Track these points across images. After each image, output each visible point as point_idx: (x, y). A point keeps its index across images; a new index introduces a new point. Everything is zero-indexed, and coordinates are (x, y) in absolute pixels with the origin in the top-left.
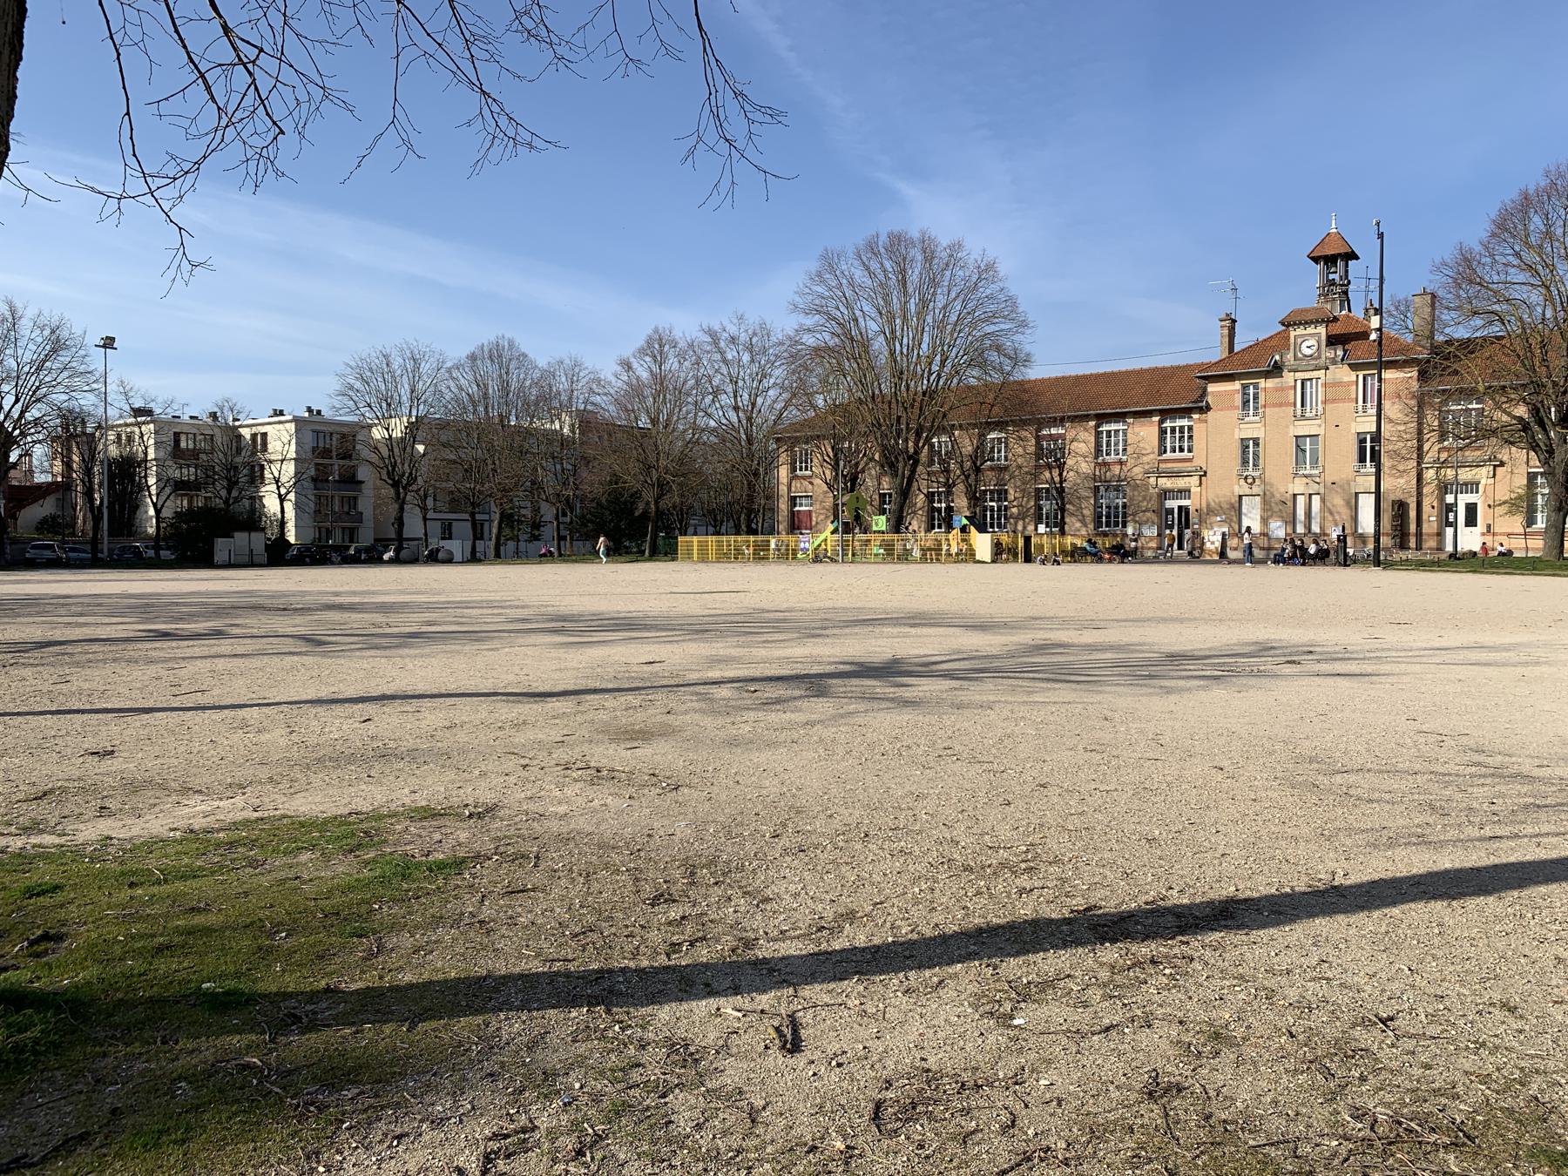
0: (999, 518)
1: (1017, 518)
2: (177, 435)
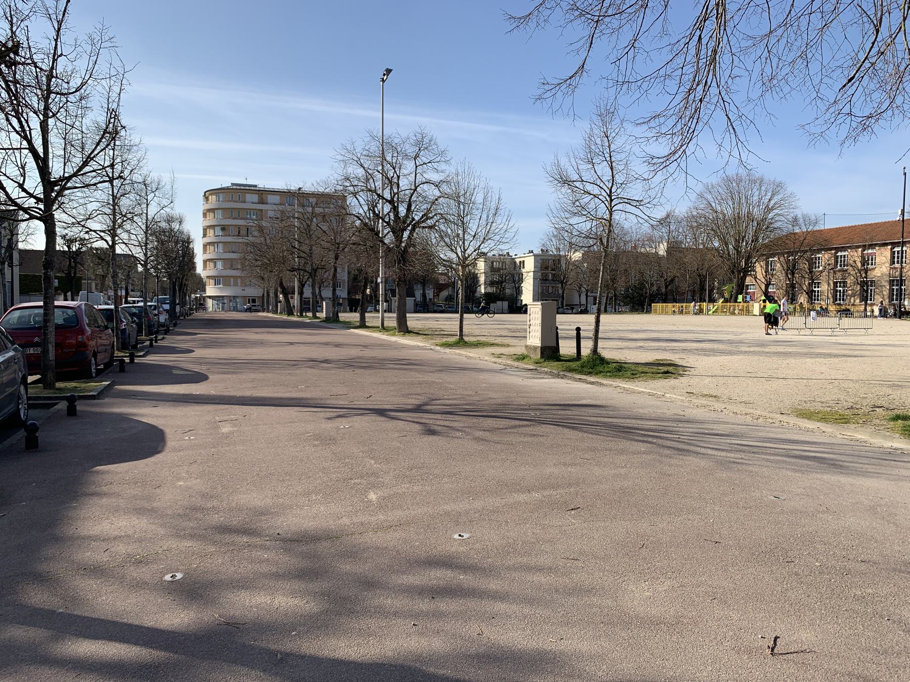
0: (843, 296)
1: (851, 296)
2: (492, 263)
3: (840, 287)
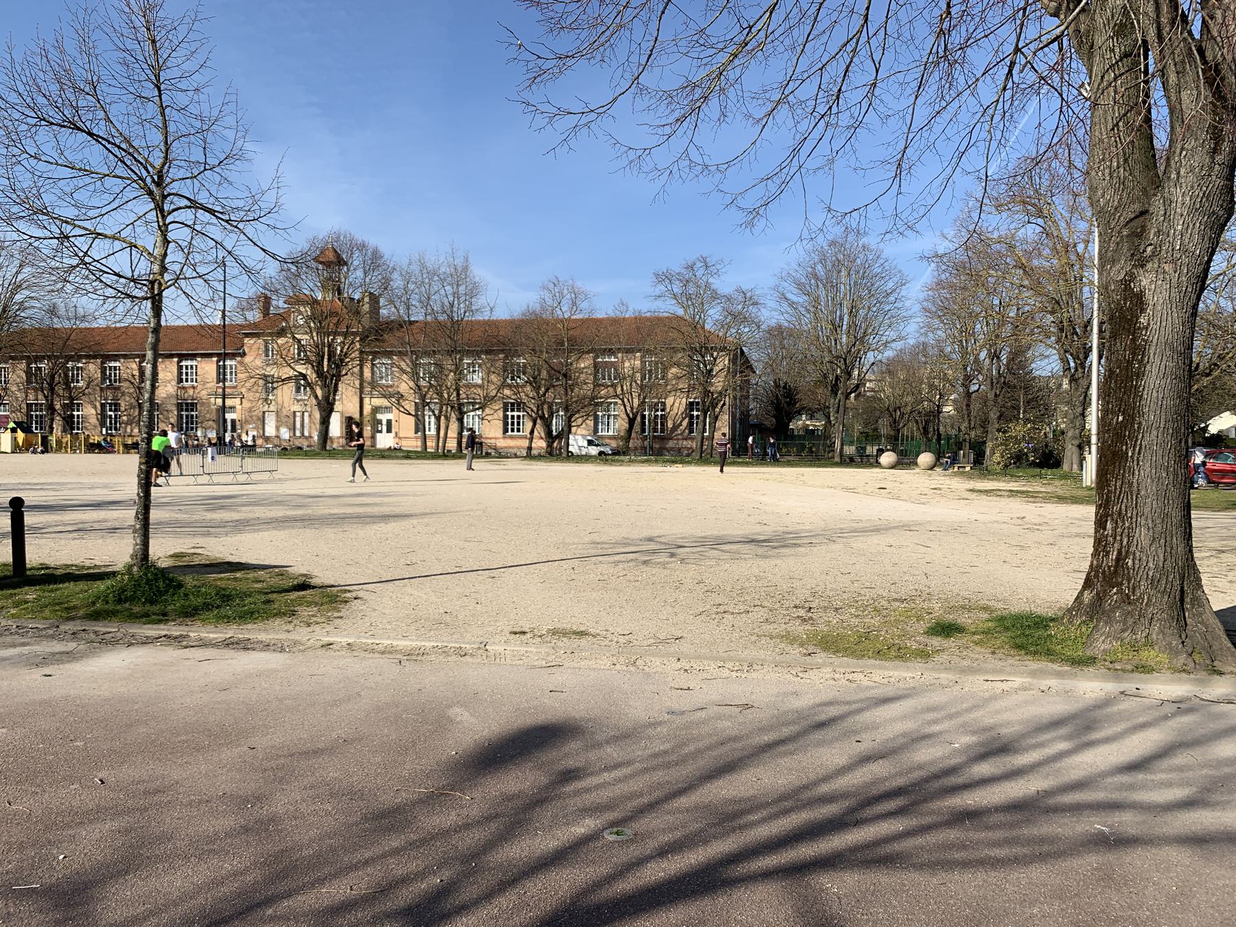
0: (116, 423)
1: (127, 424)
3: (110, 410)
